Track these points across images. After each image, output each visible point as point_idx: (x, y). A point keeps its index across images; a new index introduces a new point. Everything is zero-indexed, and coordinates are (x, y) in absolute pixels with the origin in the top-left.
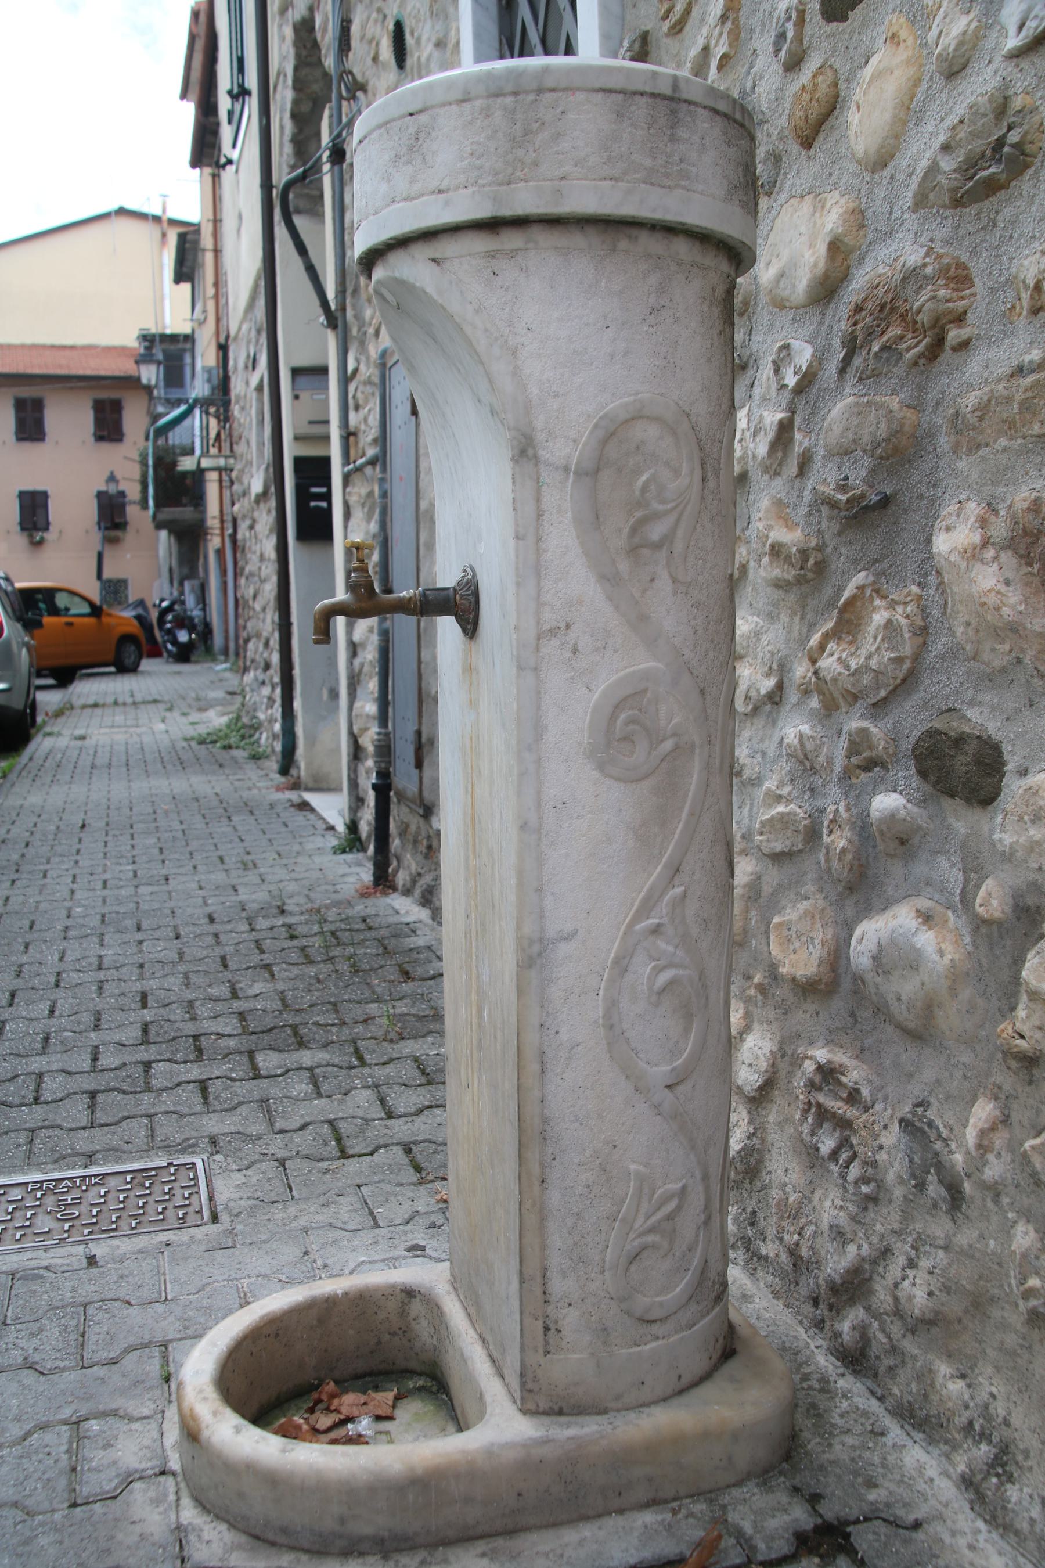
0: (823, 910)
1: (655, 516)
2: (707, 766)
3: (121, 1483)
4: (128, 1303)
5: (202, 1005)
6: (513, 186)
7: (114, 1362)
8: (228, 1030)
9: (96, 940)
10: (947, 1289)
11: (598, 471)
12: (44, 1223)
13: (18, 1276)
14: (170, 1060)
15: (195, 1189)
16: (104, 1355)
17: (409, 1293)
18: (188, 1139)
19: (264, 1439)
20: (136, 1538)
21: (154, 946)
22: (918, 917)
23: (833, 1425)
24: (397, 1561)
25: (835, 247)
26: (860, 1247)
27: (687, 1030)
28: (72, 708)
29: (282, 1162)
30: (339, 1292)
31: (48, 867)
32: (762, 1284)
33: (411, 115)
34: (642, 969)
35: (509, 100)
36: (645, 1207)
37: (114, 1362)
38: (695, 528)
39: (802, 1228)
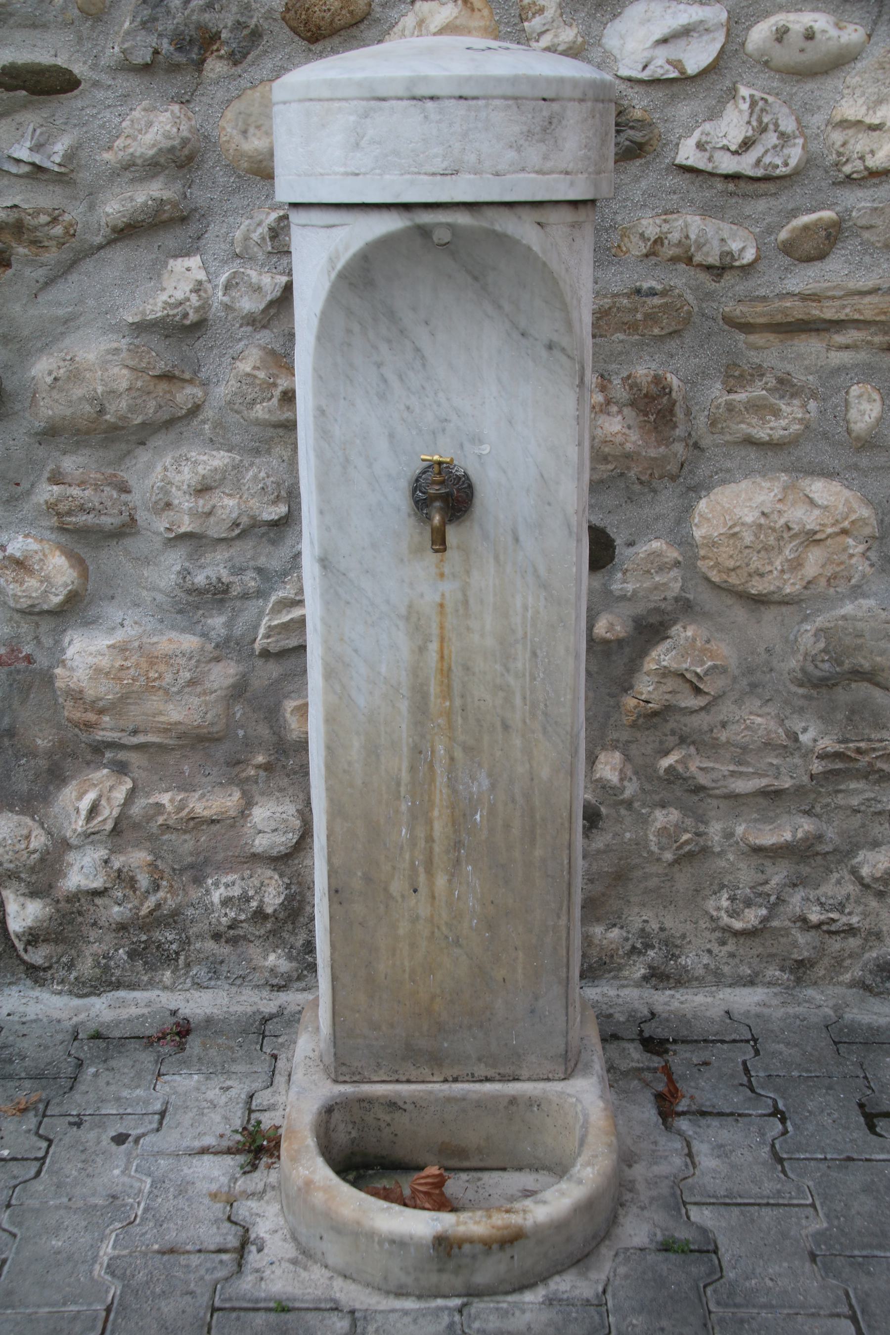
33: (544, 100)
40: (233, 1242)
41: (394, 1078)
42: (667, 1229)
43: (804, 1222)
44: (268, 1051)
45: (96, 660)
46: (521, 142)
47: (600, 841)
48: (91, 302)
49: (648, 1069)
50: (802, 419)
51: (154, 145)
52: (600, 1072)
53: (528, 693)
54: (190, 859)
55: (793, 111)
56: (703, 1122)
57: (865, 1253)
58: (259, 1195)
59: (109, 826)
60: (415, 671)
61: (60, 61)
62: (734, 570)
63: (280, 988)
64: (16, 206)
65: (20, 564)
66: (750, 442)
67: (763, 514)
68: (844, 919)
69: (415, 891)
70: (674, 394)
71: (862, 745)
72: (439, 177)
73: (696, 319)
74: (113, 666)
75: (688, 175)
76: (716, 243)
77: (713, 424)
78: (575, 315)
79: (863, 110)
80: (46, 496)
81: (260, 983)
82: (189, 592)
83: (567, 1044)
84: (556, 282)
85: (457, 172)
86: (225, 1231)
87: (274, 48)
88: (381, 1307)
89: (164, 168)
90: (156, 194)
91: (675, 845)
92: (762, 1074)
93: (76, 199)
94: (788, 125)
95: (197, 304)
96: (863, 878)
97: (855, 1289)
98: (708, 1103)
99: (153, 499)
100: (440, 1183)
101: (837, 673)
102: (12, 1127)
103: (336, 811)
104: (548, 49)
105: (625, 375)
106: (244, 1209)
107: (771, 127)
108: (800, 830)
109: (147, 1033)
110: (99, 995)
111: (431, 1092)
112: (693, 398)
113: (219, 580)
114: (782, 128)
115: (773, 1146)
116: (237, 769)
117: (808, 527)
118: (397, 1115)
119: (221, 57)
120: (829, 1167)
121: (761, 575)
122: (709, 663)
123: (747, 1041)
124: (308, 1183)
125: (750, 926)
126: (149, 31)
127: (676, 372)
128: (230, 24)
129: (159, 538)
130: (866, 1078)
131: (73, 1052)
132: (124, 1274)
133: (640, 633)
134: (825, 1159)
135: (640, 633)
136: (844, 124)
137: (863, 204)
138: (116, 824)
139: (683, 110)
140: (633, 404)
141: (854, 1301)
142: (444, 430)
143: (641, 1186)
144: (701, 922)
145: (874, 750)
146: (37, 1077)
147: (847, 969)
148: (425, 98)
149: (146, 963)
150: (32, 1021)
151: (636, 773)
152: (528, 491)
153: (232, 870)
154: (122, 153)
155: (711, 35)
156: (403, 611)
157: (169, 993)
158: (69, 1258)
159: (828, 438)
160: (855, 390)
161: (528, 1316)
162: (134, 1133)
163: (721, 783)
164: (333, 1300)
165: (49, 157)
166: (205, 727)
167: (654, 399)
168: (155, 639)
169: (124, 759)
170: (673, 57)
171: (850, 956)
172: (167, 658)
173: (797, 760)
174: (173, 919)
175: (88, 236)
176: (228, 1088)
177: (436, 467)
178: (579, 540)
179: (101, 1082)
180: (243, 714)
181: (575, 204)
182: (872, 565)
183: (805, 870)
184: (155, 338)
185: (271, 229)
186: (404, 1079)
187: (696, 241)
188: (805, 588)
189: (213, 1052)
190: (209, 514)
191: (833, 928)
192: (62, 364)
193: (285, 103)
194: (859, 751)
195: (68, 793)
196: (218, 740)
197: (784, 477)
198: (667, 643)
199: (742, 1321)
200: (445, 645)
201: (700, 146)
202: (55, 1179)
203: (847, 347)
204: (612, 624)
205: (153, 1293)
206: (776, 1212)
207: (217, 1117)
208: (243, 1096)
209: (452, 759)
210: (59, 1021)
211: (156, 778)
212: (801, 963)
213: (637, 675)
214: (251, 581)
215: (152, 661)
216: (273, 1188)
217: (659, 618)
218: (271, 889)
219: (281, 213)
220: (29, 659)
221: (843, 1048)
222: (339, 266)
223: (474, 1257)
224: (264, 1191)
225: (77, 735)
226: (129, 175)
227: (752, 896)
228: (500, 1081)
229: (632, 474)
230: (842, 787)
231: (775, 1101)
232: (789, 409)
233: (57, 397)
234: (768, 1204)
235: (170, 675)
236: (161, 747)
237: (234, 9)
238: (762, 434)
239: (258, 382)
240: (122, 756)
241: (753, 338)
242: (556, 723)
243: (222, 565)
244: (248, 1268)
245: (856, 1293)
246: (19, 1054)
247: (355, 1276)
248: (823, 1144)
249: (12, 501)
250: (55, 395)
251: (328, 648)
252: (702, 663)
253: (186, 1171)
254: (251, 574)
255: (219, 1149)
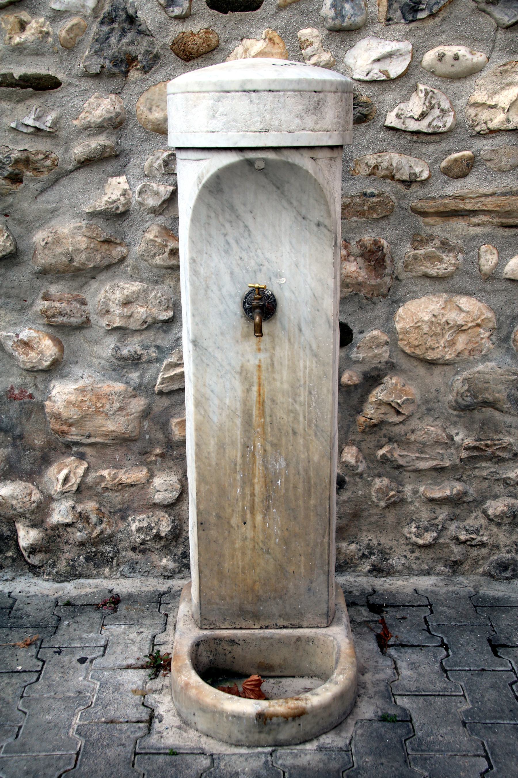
33: (315, 92)
40: (145, 717)
41: (234, 626)
42: (384, 709)
43: (459, 705)
44: (163, 612)
45: (67, 397)
46: (303, 114)
47: (345, 495)
48: (66, 201)
49: (372, 621)
50: (455, 264)
51: (101, 117)
52: (346, 623)
53: (307, 414)
54: (119, 506)
55: (448, 98)
56: (403, 650)
57: (492, 721)
58: (159, 691)
59: (75, 488)
60: (245, 403)
61: (50, 73)
62: (418, 346)
63: (169, 577)
64: (26, 150)
65: (26, 344)
66: (426, 276)
67: (434, 315)
68: (479, 538)
69: (245, 523)
70: (385, 250)
71: (489, 442)
72: (258, 133)
73: (396, 209)
74: (77, 400)
75: (391, 132)
76: (407, 168)
77: (406, 266)
78: (332, 207)
79: (486, 97)
80: (41, 307)
81: (158, 574)
82: (119, 359)
83: (328, 607)
84: (322, 190)
85: (268, 130)
86: (141, 711)
87: (167, 64)
88: (227, 752)
89: (106, 129)
90: (102, 143)
91: (386, 498)
92: (435, 624)
93: (58, 146)
94: (445, 105)
95: (124, 202)
96: (489, 516)
97: (487, 741)
98: (405, 640)
99: (100, 308)
100: (259, 684)
101: (475, 403)
102: (23, 654)
103: (201, 479)
104: (315, 65)
105: (358, 239)
106: (151, 699)
107: (436, 106)
108: (455, 489)
109: (96, 602)
110: (69, 581)
111: (253, 634)
112: (395, 252)
113: (136, 352)
114: (442, 107)
115: (441, 663)
116: (145, 457)
117: (458, 323)
118: (235, 647)
119: (138, 69)
120: (472, 675)
121: (433, 349)
122: (405, 398)
123: (426, 606)
124: (187, 684)
125: (427, 542)
126: (99, 56)
127: (386, 238)
128: (142, 52)
129: (102, 330)
130: (491, 625)
131: (55, 613)
132: (86, 734)
133: (367, 381)
134: (470, 670)
135: (367, 381)
136: (476, 105)
137: (486, 148)
138: (78, 487)
139: (389, 97)
140: (362, 255)
141: (487, 748)
142: (260, 270)
143: (369, 686)
144: (401, 540)
145: (495, 445)
146: (36, 626)
147: (481, 566)
148: (251, 91)
149: (95, 564)
150: (32, 596)
151: (365, 458)
152: (306, 303)
153: (142, 512)
154: (83, 121)
155: (403, 57)
156: (238, 369)
157: (108, 581)
158: (56, 726)
159: (469, 274)
160: (483, 248)
161: (308, 757)
162: (90, 657)
163: (411, 464)
164: (200, 748)
165: (44, 123)
166: (128, 434)
167: (374, 253)
168: (100, 385)
169: (83, 451)
170: (383, 69)
171: (482, 559)
172: (107, 396)
173: (453, 451)
174: (110, 539)
175: (65, 166)
176: (141, 633)
177: (257, 290)
178: (334, 330)
179: (71, 629)
180: (149, 426)
181: (332, 148)
182: (493, 344)
183: (458, 511)
184: (101, 220)
185: (164, 161)
186: (239, 627)
187: (396, 167)
188: (457, 356)
189: (132, 613)
190: (130, 316)
191: (473, 543)
192: (50, 235)
193: (174, 94)
194: (487, 445)
195: (52, 470)
196: (135, 440)
197: (445, 295)
198: (382, 387)
199: (426, 759)
200: (261, 388)
201: (398, 116)
202: (47, 683)
203: (479, 225)
204: (351, 376)
205: (102, 744)
206: (444, 699)
207: (135, 649)
208: (150, 637)
209: (265, 450)
210: (47, 596)
211: (100, 461)
212: (455, 563)
213: (365, 404)
214: (153, 353)
215: (99, 397)
216: (167, 687)
217: (377, 373)
218: (164, 523)
219: (170, 152)
220: (31, 396)
221: (479, 609)
222: (204, 181)
223: (279, 725)
224: (162, 689)
225: (57, 438)
226: (87, 133)
227: (428, 525)
228: (291, 628)
229: (362, 294)
230: (478, 465)
231: (442, 638)
232: (447, 259)
233: (47, 253)
234: (439, 695)
235: (109, 405)
236: (104, 445)
237: (145, 44)
238: (433, 272)
239: (157, 244)
240: (82, 449)
241: (428, 220)
242: (322, 430)
243: (137, 345)
244: (154, 731)
245: (488, 744)
246: (26, 614)
247: (213, 735)
248: (469, 662)
249: (22, 310)
250: (46, 251)
251: (197, 390)
252: (401, 397)
253: (119, 678)
254: (153, 349)
255: (137, 666)
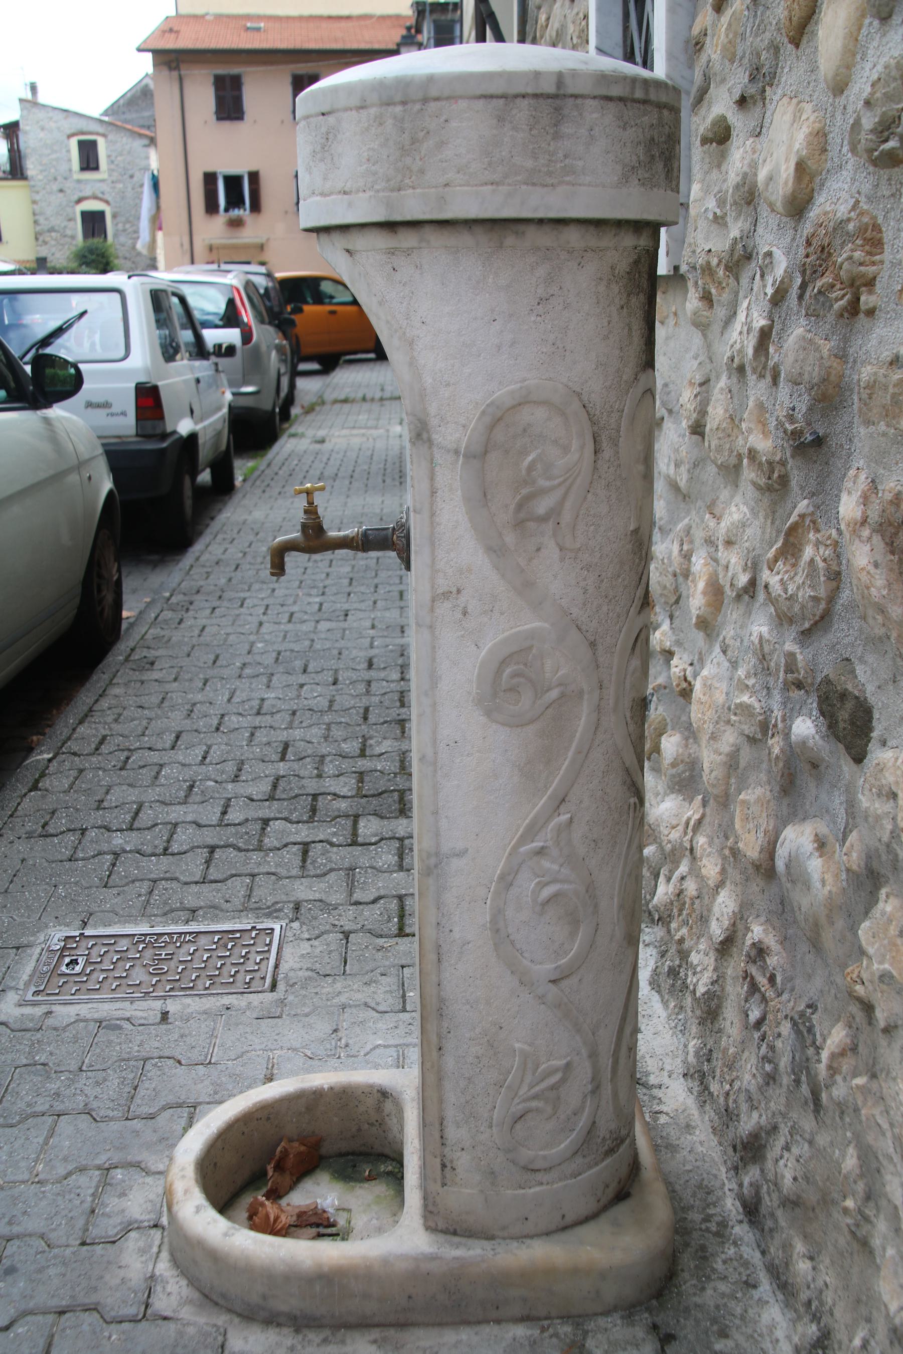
0: (769, 801)
1: (543, 492)
2: (599, 709)
3: (122, 1230)
4: (179, 1062)
5: (331, 761)
6: (402, 193)
7: (152, 1117)
8: (344, 791)
9: (264, 680)
10: (807, 1178)
11: (486, 452)
12: (139, 975)
13: (104, 1024)
14: (286, 819)
15: (266, 955)
16: (145, 1110)
17: (384, 1094)
18: (277, 903)
19: (215, 1221)
20: (118, 1281)
21: (312, 690)
22: (815, 841)
23: (714, 1270)
24: (305, 1336)
25: (801, 167)
26: (761, 1115)
27: (573, 935)
28: (323, 403)
29: (347, 935)
30: (326, 1087)
31: (247, 594)
32: (707, 1118)
33: (323, 114)
34: (526, 884)
35: (399, 109)
36: (528, 1079)
37: (152, 1117)
38: (585, 498)
39: (733, 1081)
